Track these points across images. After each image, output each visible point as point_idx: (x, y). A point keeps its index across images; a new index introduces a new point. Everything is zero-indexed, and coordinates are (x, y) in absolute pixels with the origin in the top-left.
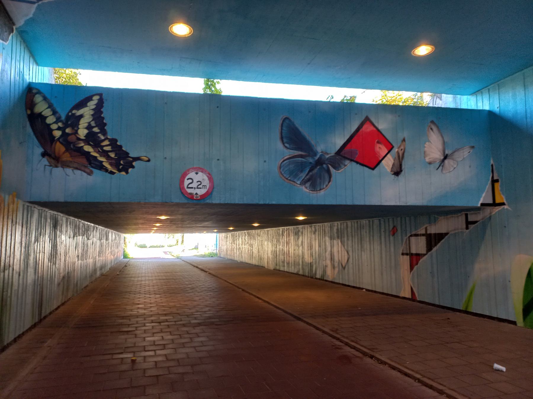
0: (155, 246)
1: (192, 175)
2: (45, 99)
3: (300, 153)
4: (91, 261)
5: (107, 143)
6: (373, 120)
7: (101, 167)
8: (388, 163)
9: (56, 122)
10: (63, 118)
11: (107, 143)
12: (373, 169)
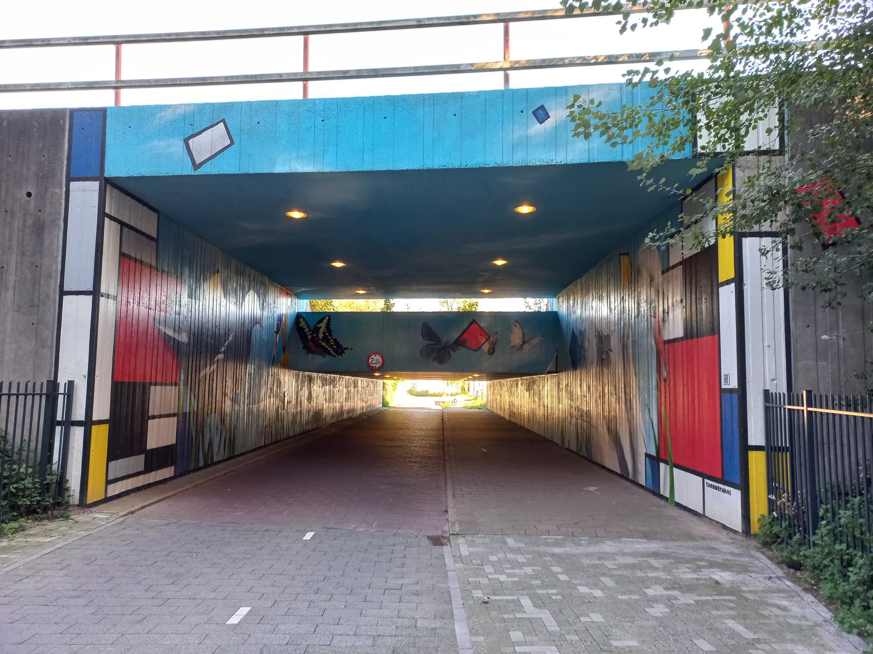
0: (436, 393)
1: (373, 356)
2: (304, 320)
3: (432, 342)
4: (337, 405)
5: (332, 340)
6: (477, 321)
7: (329, 353)
8: (486, 347)
9: (309, 331)
10: (312, 329)
11: (332, 340)
12: (477, 351)
